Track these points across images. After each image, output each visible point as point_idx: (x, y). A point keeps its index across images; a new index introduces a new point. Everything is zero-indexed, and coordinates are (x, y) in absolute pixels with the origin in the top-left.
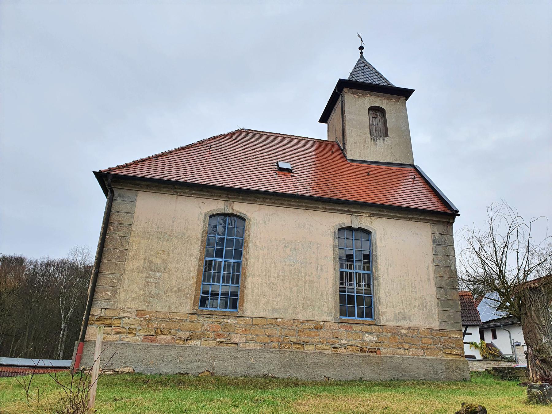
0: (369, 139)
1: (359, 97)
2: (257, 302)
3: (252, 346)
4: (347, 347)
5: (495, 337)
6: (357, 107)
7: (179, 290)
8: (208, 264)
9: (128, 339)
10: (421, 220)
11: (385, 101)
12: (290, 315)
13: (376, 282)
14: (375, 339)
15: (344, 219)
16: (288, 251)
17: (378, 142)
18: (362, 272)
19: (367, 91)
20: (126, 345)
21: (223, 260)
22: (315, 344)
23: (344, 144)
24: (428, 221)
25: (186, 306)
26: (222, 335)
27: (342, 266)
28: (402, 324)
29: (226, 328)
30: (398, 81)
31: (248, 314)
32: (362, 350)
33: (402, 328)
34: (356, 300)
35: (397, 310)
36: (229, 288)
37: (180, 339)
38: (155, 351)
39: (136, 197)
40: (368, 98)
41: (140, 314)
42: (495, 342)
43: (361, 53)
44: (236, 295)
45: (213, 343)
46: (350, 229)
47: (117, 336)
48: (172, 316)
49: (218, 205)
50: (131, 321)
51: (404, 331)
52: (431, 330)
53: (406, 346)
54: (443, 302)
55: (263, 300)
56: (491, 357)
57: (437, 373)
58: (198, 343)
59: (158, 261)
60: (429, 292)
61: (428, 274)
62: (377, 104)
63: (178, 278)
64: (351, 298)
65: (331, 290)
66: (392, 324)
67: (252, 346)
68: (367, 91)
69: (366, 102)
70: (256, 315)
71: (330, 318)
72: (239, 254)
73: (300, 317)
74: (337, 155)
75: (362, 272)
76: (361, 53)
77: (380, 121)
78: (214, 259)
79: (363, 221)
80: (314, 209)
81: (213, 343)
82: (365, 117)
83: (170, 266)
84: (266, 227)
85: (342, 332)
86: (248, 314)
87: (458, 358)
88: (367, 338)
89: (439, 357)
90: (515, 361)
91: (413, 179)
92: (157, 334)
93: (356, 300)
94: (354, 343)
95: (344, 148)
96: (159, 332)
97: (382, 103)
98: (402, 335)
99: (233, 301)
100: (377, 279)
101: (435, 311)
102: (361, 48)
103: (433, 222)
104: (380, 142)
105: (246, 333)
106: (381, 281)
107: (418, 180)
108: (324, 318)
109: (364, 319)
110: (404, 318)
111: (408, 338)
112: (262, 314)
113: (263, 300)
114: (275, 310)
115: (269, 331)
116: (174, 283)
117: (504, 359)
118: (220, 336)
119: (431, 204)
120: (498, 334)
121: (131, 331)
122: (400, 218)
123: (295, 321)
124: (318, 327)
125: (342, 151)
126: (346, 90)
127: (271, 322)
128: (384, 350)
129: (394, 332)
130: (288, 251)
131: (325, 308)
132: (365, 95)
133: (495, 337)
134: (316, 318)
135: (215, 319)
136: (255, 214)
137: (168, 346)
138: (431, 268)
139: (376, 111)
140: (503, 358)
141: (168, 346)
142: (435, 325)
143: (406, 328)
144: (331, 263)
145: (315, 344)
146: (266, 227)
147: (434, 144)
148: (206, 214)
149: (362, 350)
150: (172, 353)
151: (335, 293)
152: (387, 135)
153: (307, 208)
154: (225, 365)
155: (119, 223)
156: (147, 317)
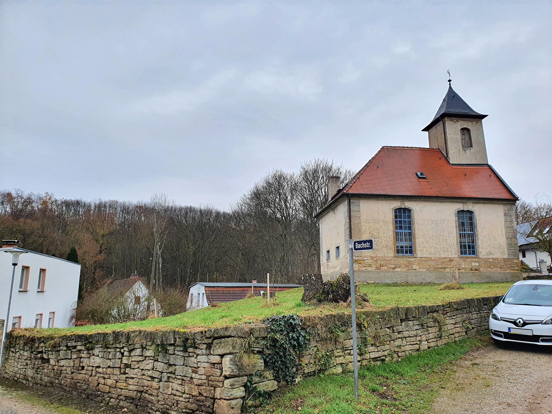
0: (462, 150)
1: (455, 122)
2: (422, 251)
3: (422, 270)
4: (464, 269)
5: (524, 256)
6: (453, 129)
7: (387, 247)
8: (397, 234)
9: (369, 269)
10: (498, 204)
11: (470, 124)
12: (438, 256)
13: (477, 238)
14: (478, 264)
15: (460, 206)
16: (433, 224)
17: (467, 151)
18: (470, 232)
19: (456, 113)
20: (363, 271)
21: (403, 231)
22: (450, 268)
23: (447, 154)
24: (502, 204)
25: (391, 253)
26: (408, 265)
27: (460, 231)
28: (490, 257)
29: (409, 262)
30: (478, 109)
31: (419, 256)
32: (471, 270)
33: (490, 259)
34: (468, 247)
35: (488, 250)
36: (407, 244)
37: (391, 268)
38: (382, 274)
39: (359, 203)
40: (459, 123)
41: (372, 258)
42: (524, 260)
43: (450, 84)
44: (411, 247)
45: (405, 270)
46: (463, 211)
47: (364, 268)
48: (386, 258)
49: (397, 204)
50: (369, 261)
51: (491, 260)
52: (504, 259)
53: (492, 267)
54: (510, 245)
55: (425, 250)
56: (524, 270)
57: (507, 279)
58: (399, 270)
59: (375, 234)
60: (503, 241)
61: (502, 231)
62: (465, 126)
63: (385, 241)
64: (465, 246)
65: (456, 243)
66: (485, 257)
67: (422, 270)
68: (456, 113)
69: (459, 125)
70: (422, 256)
71: (456, 256)
72: (410, 228)
73: (442, 256)
74: (443, 161)
75: (470, 232)
76: (450, 84)
77: (467, 137)
78: (399, 231)
79: (469, 207)
80: (445, 202)
81: (405, 270)
82: (459, 136)
83: (381, 235)
84: (421, 212)
85: (462, 262)
86: (419, 256)
87: (517, 271)
88: (474, 264)
89: (508, 271)
90: (540, 272)
91: (490, 176)
92: (381, 266)
93: (468, 247)
94: (467, 266)
95: (447, 156)
96: (381, 266)
97: (468, 125)
98: (490, 262)
99: (410, 250)
100: (477, 236)
101: (506, 250)
102: (450, 81)
103: (504, 204)
104: (468, 151)
105: (419, 264)
106: (479, 237)
107: (493, 176)
108: (454, 256)
109: (472, 255)
110: (491, 254)
111: (494, 263)
112: (425, 256)
113: (425, 250)
114: (430, 254)
115: (429, 263)
116: (384, 243)
117: (532, 270)
118: (408, 266)
119: (506, 196)
120: (527, 254)
121: (370, 266)
122: (487, 203)
123: (440, 258)
124: (451, 260)
125: (446, 159)
126: (446, 119)
127: (430, 259)
128: (481, 269)
129: (486, 261)
130: (433, 224)
131: (453, 252)
132: (458, 121)
133: (524, 256)
134: (450, 256)
135: (404, 259)
136: (414, 206)
137: (387, 271)
138: (504, 228)
139: (465, 131)
140: (532, 270)
141: (387, 271)
142: (506, 256)
143: (492, 259)
144: (454, 230)
145: (450, 268)
146: (421, 212)
147: (501, 148)
148: (392, 209)
149: (471, 270)
150: (389, 274)
151: (457, 244)
152: (471, 146)
153: (441, 202)
154: (411, 279)
155: (355, 216)
156: (375, 259)
